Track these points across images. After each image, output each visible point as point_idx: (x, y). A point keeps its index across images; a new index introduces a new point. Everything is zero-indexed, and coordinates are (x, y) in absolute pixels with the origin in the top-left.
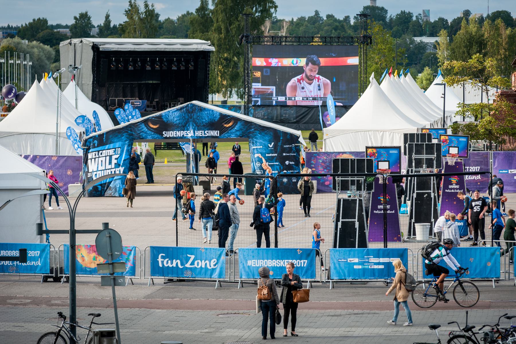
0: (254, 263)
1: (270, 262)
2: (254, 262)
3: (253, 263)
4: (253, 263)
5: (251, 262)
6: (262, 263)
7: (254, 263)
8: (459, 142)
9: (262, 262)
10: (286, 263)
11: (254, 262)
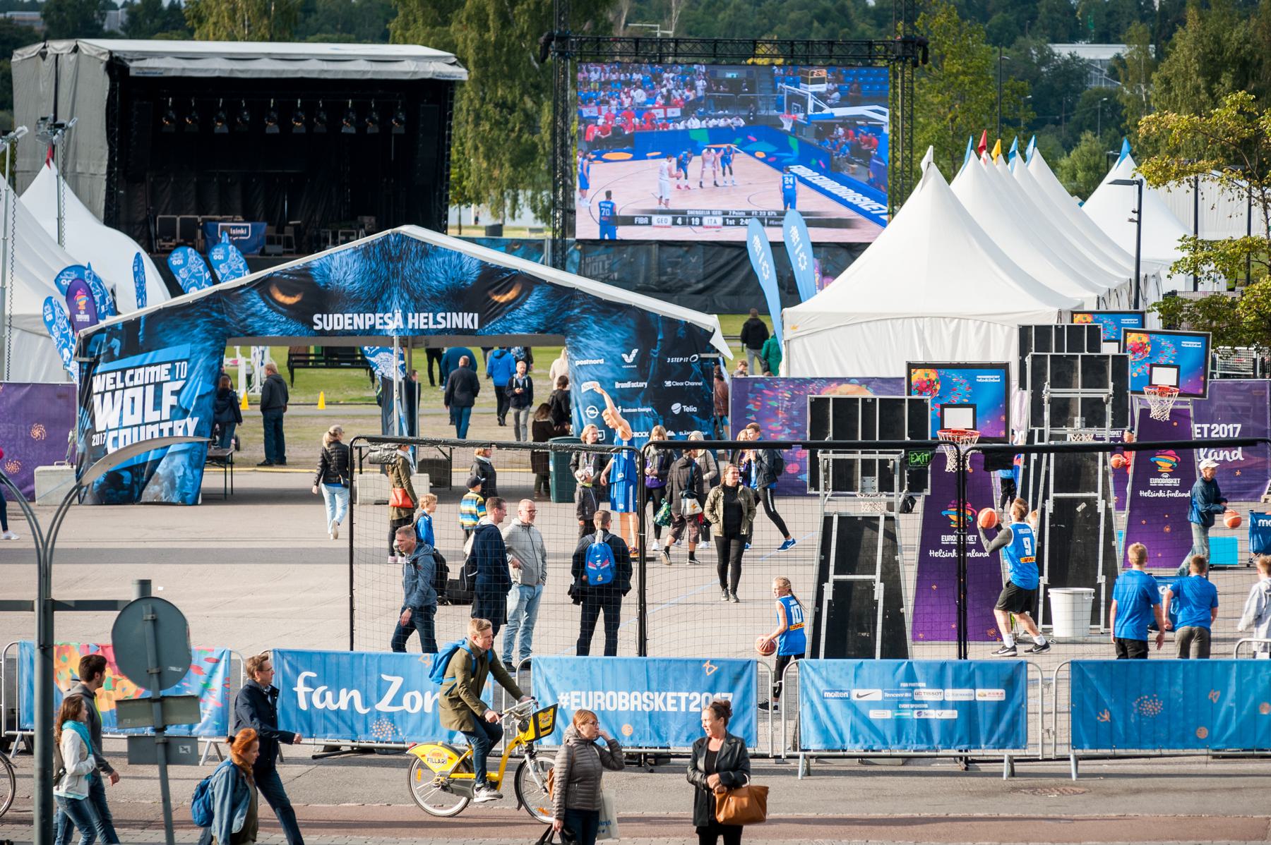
0: (578, 701)
1: (624, 697)
2: (576, 697)
3: (574, 701)
4: (574, 701)
5: (567, 698)
6: (601, 701)
7: (578, 701)
8: (1180, 350)
9: (599, 697)
10: (670, 702)
11: (576, 697)
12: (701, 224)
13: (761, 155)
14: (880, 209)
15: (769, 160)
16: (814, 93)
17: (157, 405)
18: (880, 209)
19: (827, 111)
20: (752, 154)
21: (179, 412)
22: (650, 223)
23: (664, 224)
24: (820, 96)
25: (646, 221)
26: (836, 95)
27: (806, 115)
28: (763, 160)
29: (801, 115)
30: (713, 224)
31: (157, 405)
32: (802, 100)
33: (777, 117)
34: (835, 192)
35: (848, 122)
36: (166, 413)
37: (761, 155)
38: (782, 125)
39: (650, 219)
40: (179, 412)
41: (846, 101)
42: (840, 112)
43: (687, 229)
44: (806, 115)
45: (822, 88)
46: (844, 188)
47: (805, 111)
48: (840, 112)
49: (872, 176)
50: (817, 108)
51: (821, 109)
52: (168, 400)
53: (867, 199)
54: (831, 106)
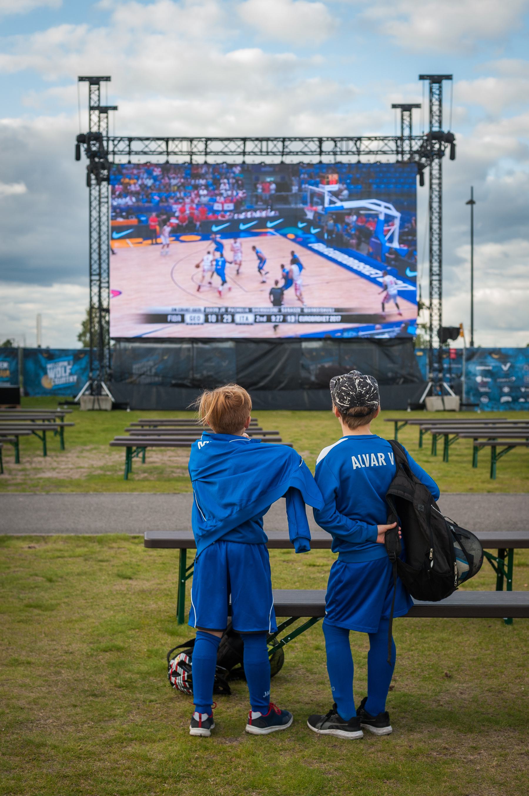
12: (233, 321)
13: (291, 236)
14: (377, 274)
15: (298, 240)
16: (330, 192)
17: (65, 372)
18: (377, 274)
19: (339, 204)
20: (285, 235)
21: (71, 374)
22: (183, 321)
23: (197, 322)
24: (334, 194)
25: (179, 318)
26: (345, 192)
27: (324, 208)
28: (294, 240)
29: (320, 208)
30: (245, 321)
31: (65, 372)
32: (321, 197)
33: (302, 210)
34: (344, 262)
35: (356, 211)
36: (67, 374)
37: (291, 236)
38: (306, 215)
39: (183, 316)
40: (71, 374)
41: (351, 198)
42: (348, 205)
43: (220, 326)
44: (324, 208)
45: (335, 187)
46: (351, 259)
47: (323, 203)
48: (348, 205)
49: (371, 250)
50: (331, 202)
51: (334, 203)
52: (68, 371)
53: (368, 267)
54: (342, 200)
